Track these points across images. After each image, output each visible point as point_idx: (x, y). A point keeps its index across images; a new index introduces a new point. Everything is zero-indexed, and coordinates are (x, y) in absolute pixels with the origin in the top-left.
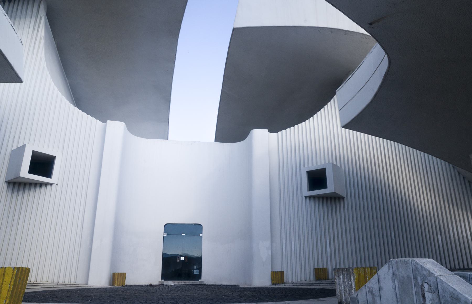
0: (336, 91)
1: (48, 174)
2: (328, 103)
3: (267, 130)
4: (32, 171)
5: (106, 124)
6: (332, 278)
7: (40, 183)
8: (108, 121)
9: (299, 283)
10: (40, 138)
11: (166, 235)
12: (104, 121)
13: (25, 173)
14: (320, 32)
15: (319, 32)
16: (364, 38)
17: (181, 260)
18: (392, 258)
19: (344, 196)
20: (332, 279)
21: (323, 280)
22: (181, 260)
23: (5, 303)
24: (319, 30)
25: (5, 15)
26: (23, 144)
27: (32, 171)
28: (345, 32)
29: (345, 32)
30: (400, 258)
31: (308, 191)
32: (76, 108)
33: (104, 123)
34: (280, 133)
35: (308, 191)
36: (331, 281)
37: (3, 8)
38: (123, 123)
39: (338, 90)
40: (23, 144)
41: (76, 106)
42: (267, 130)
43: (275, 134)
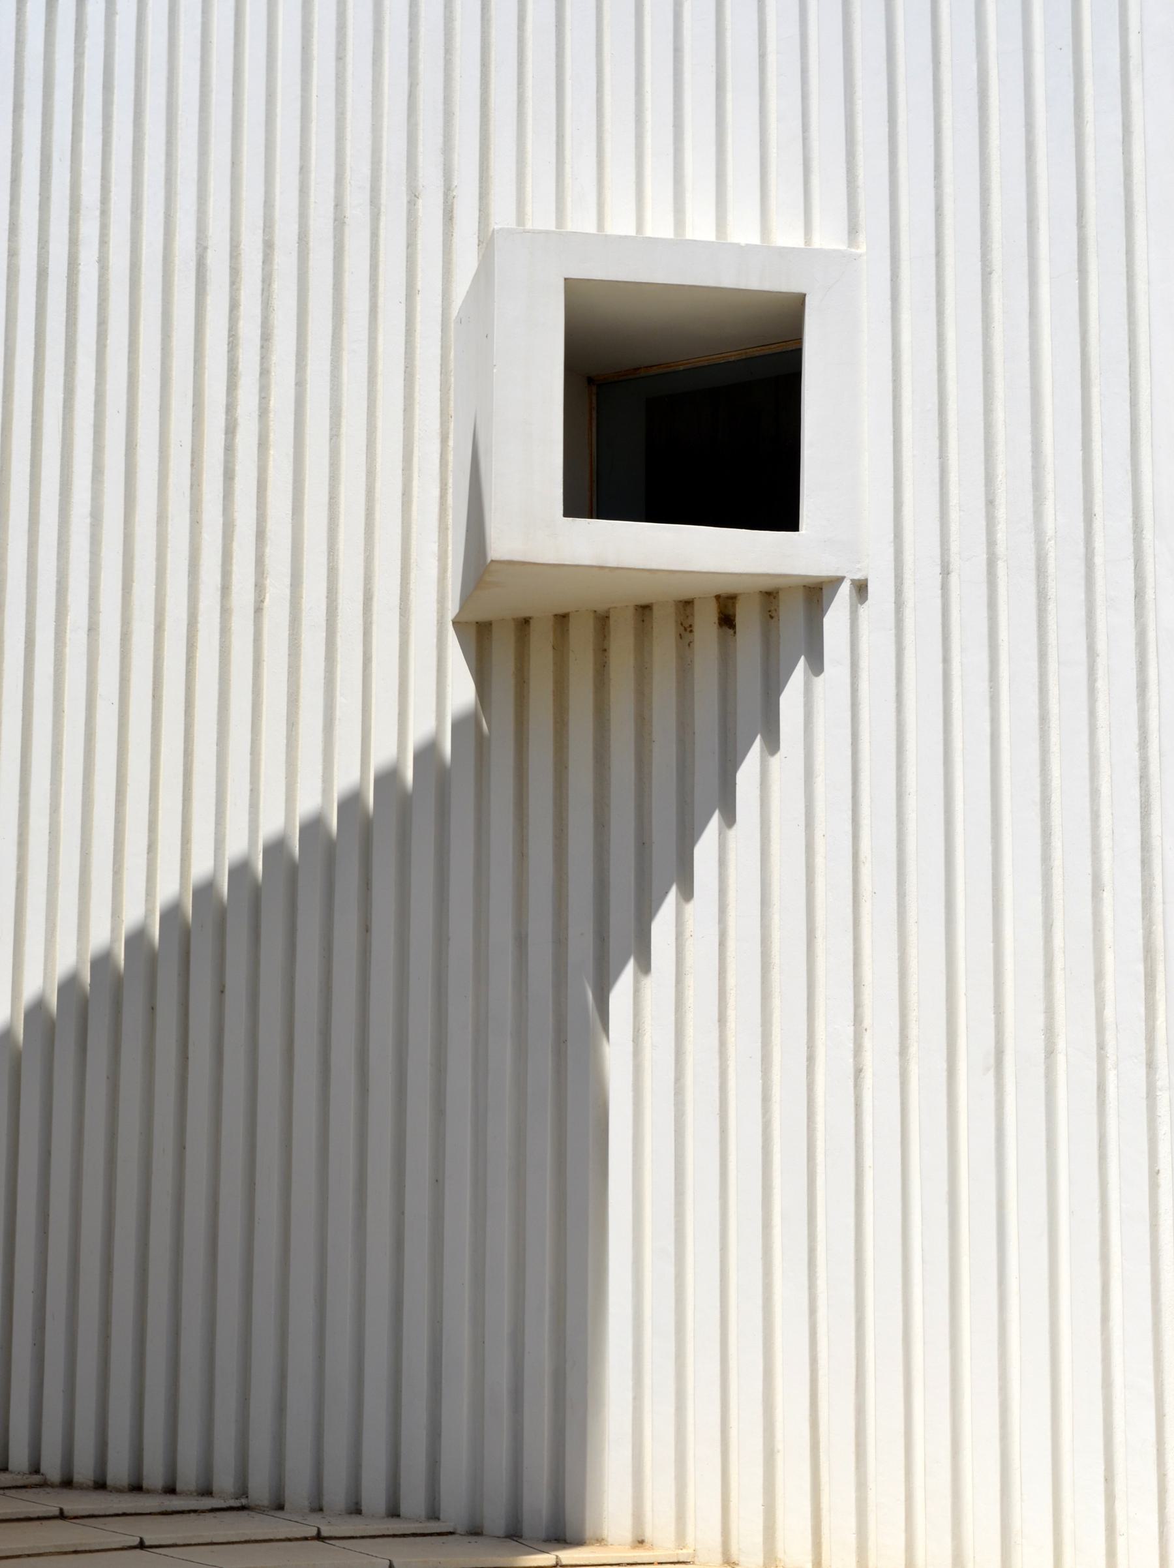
7: (768, 585)
31: (573, 288)
35: (573, 288)
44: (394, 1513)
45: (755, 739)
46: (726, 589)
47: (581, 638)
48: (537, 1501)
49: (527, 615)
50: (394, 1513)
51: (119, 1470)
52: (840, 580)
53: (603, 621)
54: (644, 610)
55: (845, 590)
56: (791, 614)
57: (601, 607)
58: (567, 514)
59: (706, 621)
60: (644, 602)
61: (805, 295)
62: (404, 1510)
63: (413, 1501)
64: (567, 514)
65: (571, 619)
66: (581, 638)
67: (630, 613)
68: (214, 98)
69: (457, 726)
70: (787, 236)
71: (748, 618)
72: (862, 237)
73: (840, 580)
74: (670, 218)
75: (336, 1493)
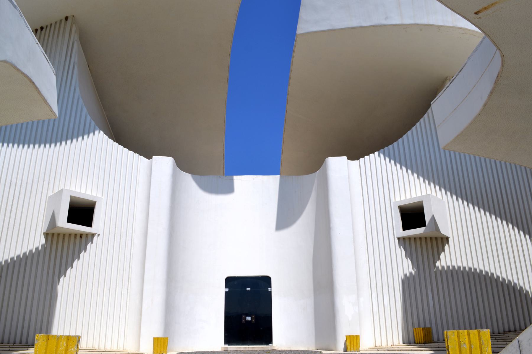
0: (431, 103)
1: (89, 223)
2: (421, 119)
3: (346, 157)
4: (70, 220)
5: (152, 160)
6: (438, 341)
7: (87, 233)
8: (154, 157)
9: (396, 347)
10: (28, 175)
11: (228, 291)
12: (149, 157)
13: (62, 222)
14: (406, 31)
15: (405, 30)
16: (463, 34)
17: (247, 320)
18: (475, 328)
19: (448, 236)
20: (438, 342)
21: (428, 343)
22: (247, 320)
23: (160, 353)
24: (404, 29)
25: (38, 44)
26: (58, 190)
27: (70, 220)
28: (438, 28)
29: (438, 28)
30: (484, 329)
31: (71, 197)
32: (116, 144)
33: (149, 159)
34: (362, 160)
35: (71, 197)
36: (438, 344)
37: (36, 35)
38: (127, 149)
39: (434, 102)
40: (58, 190)
41: (115, 141)
42: (346, 157)
43: (356, 162)
44: (20, 343)
45: (82, 251)
46: (82, 233)
47: (61, 237)
48: (30, 342)
49: (54, 233)
50: (20, 343)
51: (512, 329)
52: (96, 234)
53: (64, 235)
54: (70, 234)
55: (97, 235)
56: (90, 237)
57: (64, 233)
58: (67, 222)
59: (78, 237)
60: (59, 233)
61: (96, 202)
62: (22, 343)
63: (24, 341)
64: (67, 222)
65: (60, 235)
66: (61, 237)
67: (68, 235)
68: (415, 140)
69: (42, 246)
70: (94, 194)
71: (84, 237)
72: (103, 196)
73: (96, 234)
74: (85, 191)
75: (12, 340)
